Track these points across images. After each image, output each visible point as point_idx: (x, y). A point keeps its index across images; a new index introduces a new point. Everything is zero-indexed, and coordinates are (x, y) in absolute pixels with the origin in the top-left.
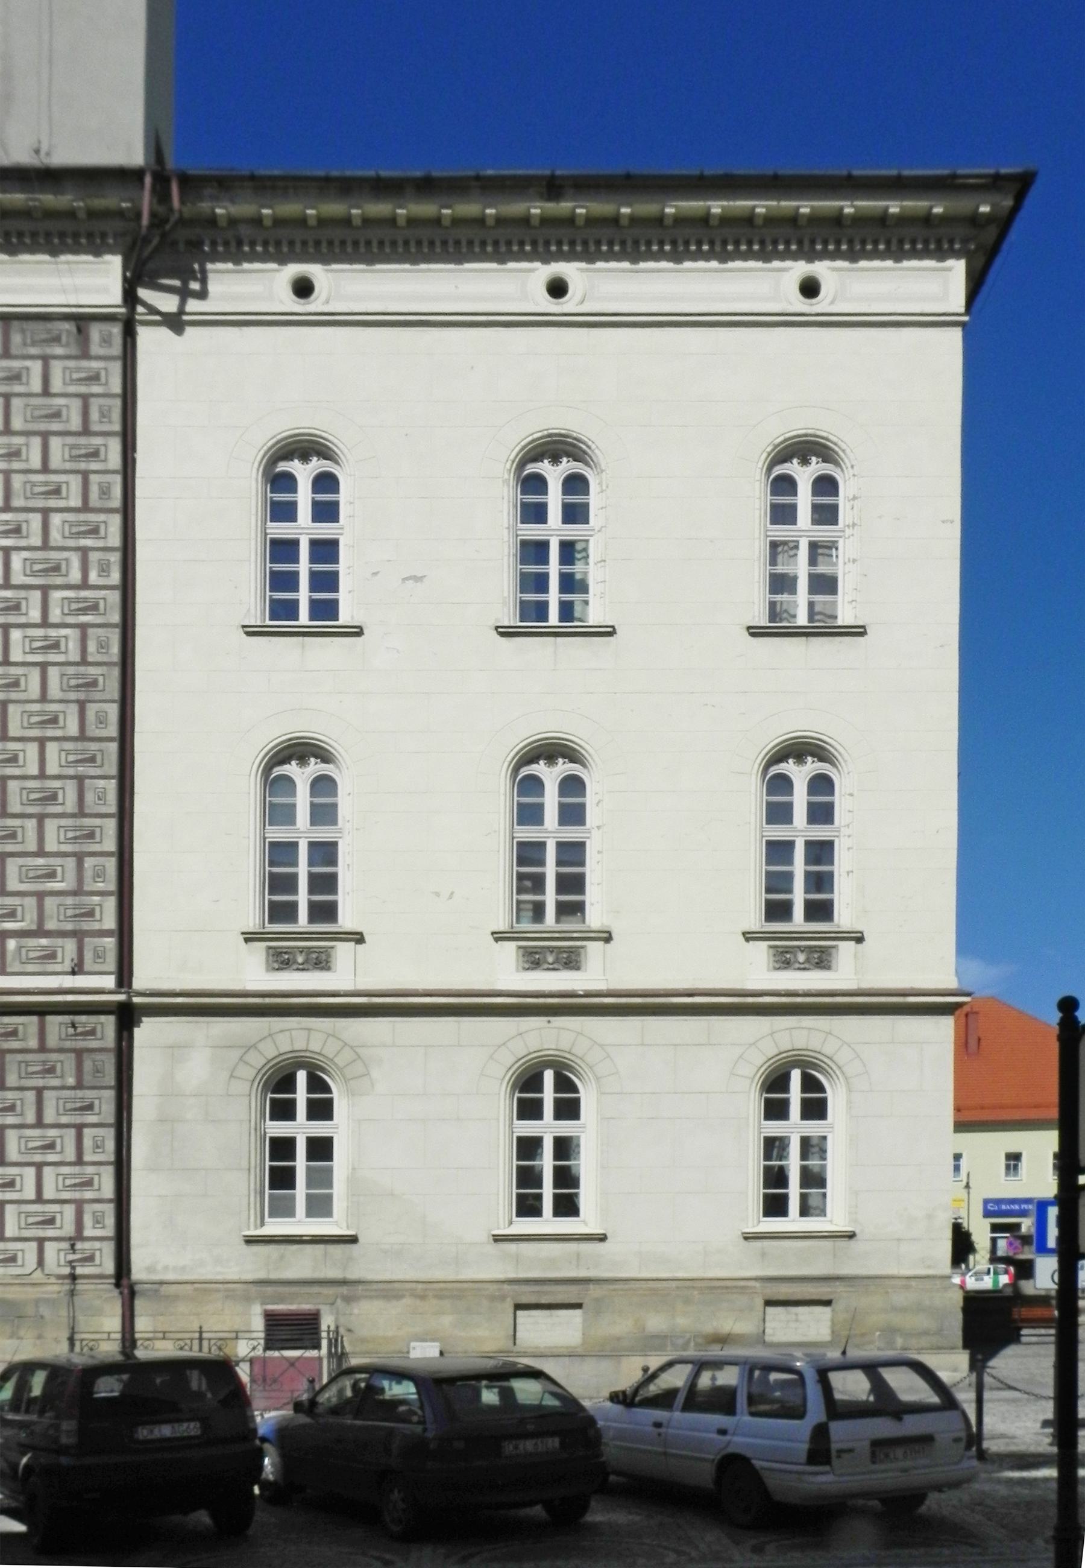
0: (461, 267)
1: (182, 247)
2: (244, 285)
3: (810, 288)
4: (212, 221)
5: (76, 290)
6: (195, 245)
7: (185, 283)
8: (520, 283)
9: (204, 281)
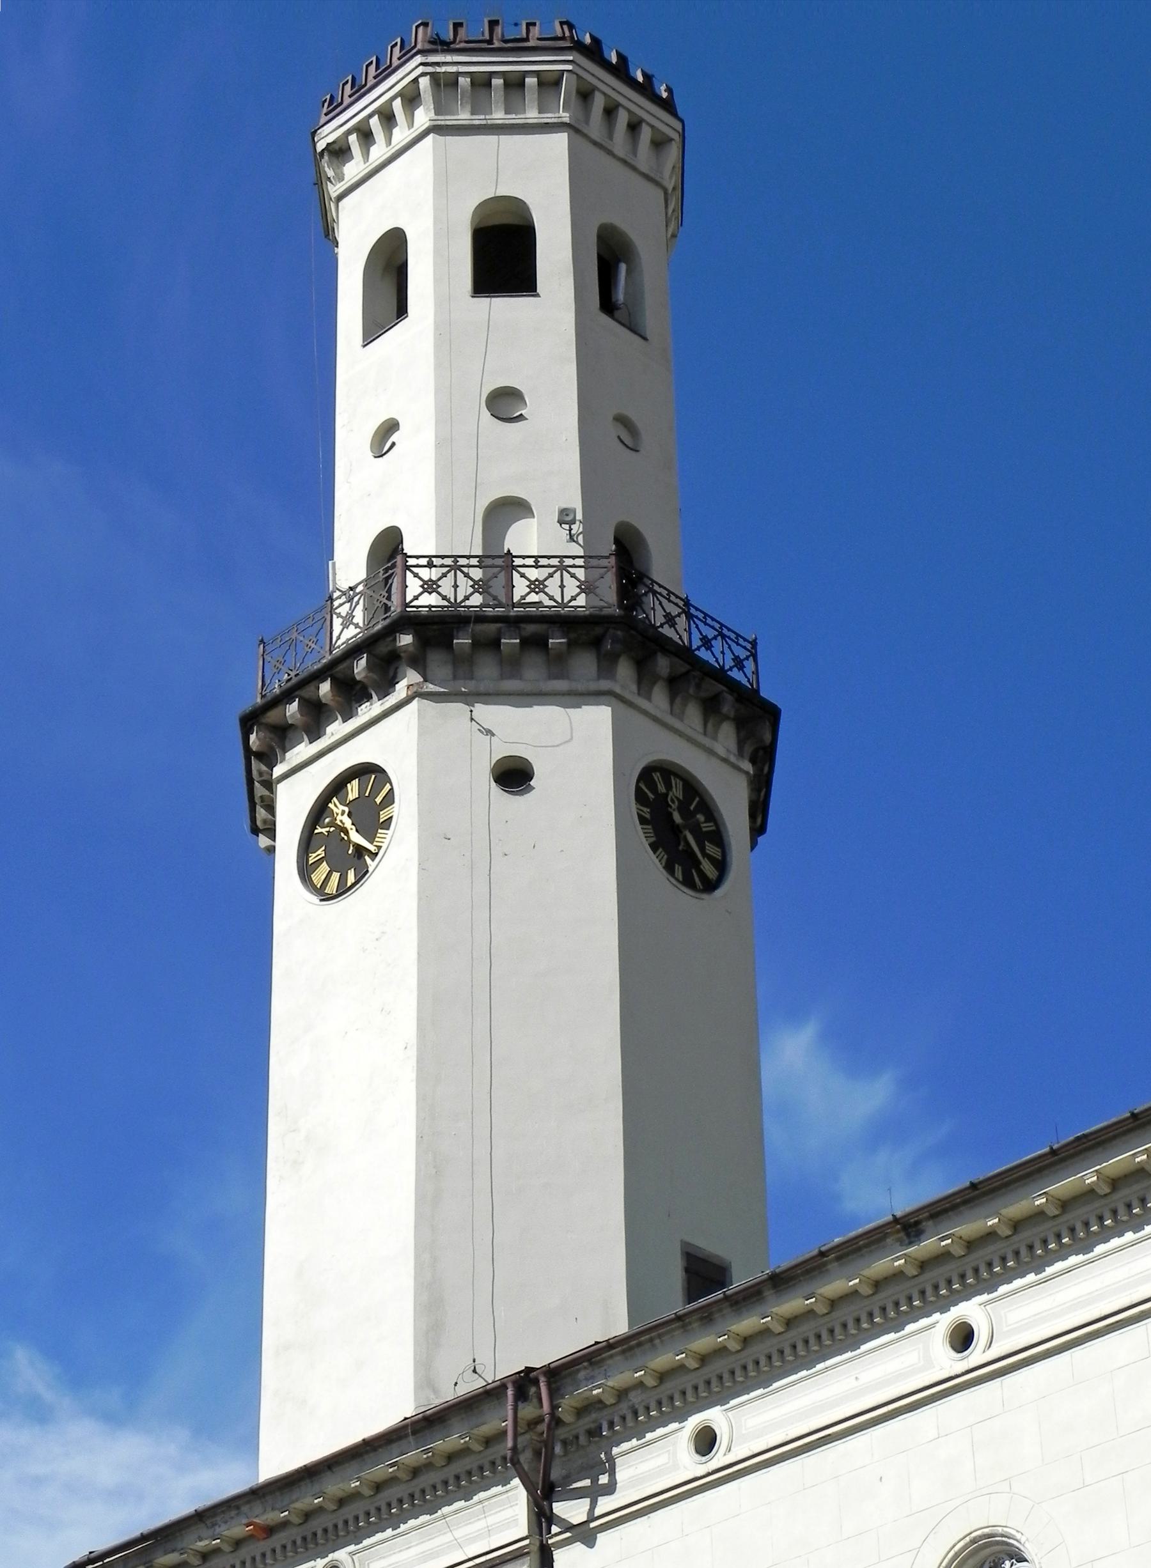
0: (858, 1352)
1: (583, 1440)
2: (651, 1461)
3: (706, 1441)
4: (598, 1404)
5: (489, 1531)
6: (594, 1433)
7: (595, 1480)
8: (916, 1351)
9: (612, 1472)
